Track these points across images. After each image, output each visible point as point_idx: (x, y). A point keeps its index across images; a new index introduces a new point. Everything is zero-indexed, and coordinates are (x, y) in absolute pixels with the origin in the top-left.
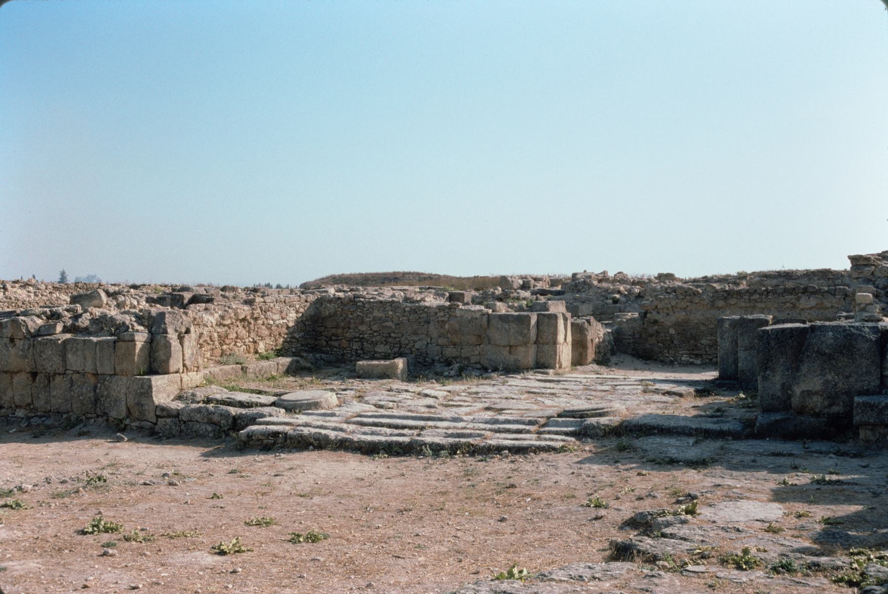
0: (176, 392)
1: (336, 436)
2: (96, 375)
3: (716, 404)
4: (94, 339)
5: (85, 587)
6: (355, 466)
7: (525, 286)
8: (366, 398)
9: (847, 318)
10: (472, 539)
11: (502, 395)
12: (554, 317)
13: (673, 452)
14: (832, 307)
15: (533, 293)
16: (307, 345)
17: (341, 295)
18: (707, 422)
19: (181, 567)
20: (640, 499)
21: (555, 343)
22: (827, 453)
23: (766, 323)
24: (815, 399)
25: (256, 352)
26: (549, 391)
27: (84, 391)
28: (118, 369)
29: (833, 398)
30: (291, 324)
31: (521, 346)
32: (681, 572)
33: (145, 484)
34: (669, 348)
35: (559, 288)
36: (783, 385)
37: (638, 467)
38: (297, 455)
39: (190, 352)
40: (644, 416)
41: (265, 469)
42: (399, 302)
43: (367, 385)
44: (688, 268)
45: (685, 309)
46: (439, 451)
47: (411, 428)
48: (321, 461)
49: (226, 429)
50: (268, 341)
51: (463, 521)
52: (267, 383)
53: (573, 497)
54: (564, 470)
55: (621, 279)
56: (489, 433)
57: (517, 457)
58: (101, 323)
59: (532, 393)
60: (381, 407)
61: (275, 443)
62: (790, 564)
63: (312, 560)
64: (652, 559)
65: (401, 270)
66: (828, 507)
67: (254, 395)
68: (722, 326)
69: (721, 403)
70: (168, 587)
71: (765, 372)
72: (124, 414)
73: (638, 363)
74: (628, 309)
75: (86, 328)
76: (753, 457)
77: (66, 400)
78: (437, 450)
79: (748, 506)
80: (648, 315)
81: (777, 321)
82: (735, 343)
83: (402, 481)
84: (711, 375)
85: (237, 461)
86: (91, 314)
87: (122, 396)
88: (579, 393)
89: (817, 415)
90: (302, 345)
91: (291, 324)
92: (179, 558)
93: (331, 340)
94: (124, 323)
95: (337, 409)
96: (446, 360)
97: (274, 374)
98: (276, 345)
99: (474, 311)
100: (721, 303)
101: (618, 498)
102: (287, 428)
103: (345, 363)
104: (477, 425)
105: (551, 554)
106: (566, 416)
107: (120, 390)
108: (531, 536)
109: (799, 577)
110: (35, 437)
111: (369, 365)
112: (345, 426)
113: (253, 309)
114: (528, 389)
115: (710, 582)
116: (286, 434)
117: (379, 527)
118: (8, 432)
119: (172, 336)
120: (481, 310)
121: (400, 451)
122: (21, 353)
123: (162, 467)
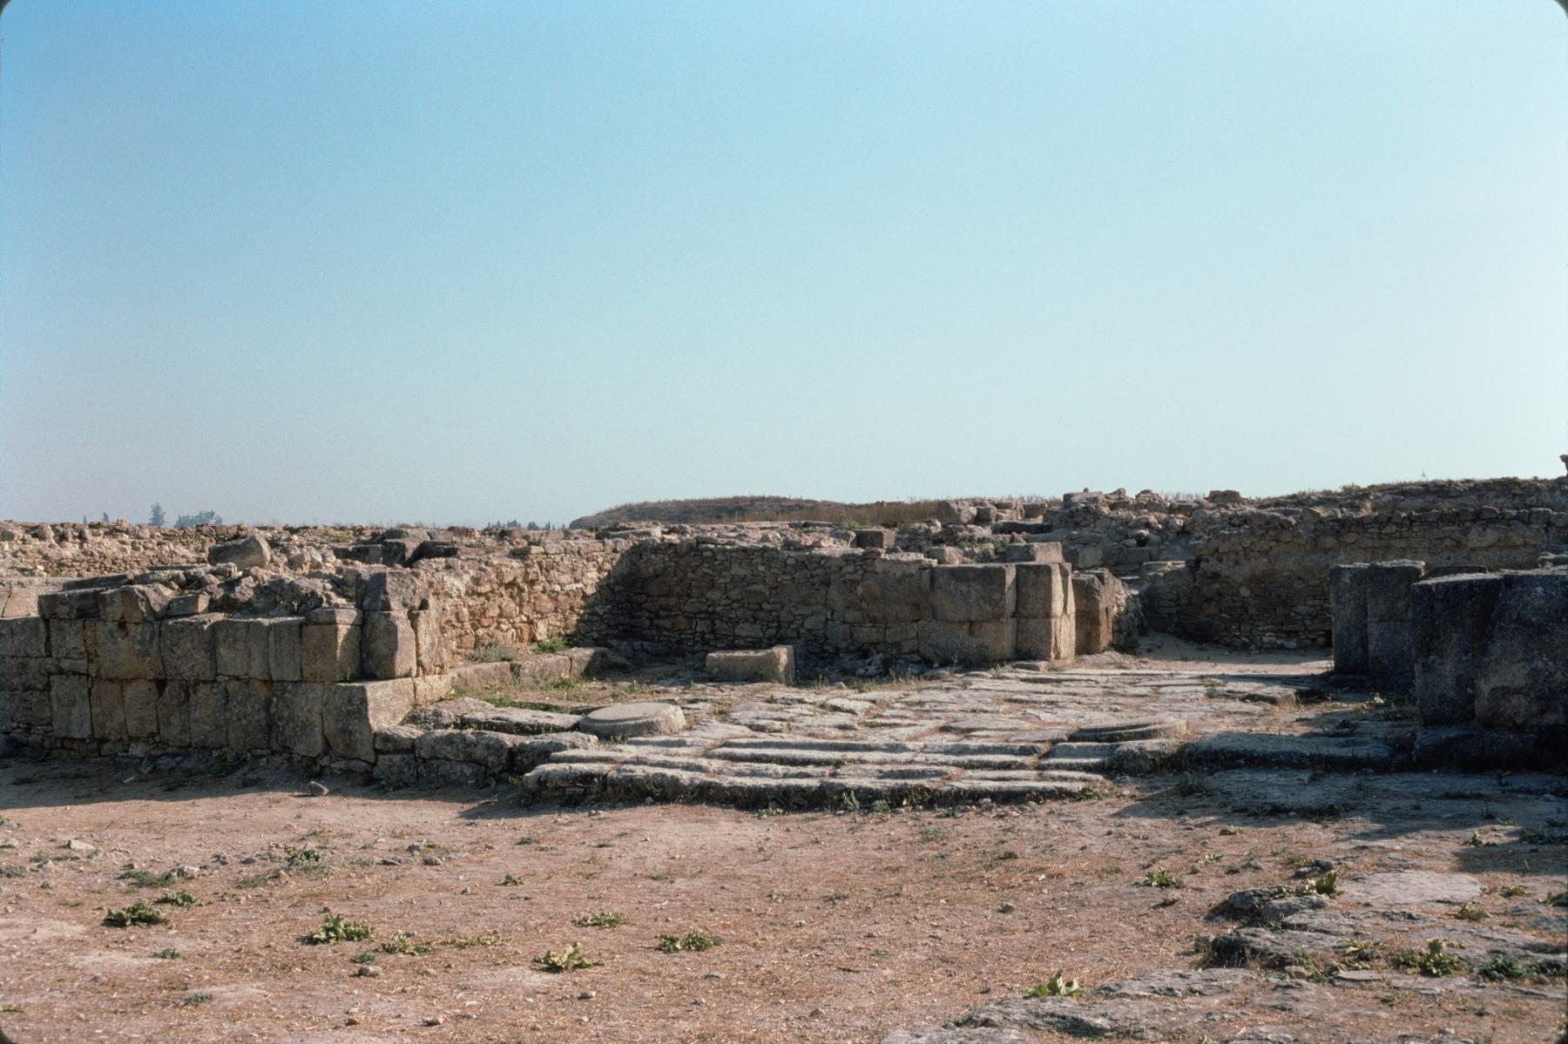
1: (692, 780)
2: (269, 682)
4: (266, 622)
5: (351, 1023)
6: (728, 831)
7: (981, 518)
9: (1556, 562)
11: (965, 706)
12: (1047, 570)
13: (1276, 796)
14: (1525, 545)
16: (617, 626)
17: (674, 538)
19: (494, 991)
20: (1232, 871)
21: (1048, 615)
22: (1539, 793)
23: (1414, 574)
24: (1515, 701)
25: (533, 640)
26: (1044, 698)
28: (306, 673)
29: (1546, 700)
30: (590, 591)
31: (989, 621)
32: (1331, 982)
33: (385, 863)
35: (1039, 520)
36: (1459, 678)
37: (1220, 821)
38: (627, 812)
39: (428, 640)
40: (1220, 736)
42: (774, 549)
43: (730, 693)
44: (1264, 479)
45: (1266, 553)
46: (871, 801)
47: (818, 763)
48: (670, 822)
49: (496, 770)
50: (552, 620)
52: (554, 691)
53: (1118, 871)
55: (1148, 502)
56: (953, 770)
57: (1007, 808)
58: (274, 594)
59: (1016, 701)
60: (761, 729)
61: (585, 794)
62: (1510, 965)
64: (1279, 964)
66: (1555, 878)
67: (540, 713)
69: (1345, 713)
70: (485, 1022)
71: (1426, 657)
73: (1187, 647)
75: (249, 603)
76: (1414, 802)
77: (217, 727)
78: (867, 799)
79: (1420, 882)
80: (1203, 565)
81: (1433, 573)
82: (1363, 609)
84: (1319, 666)
85: (526, 824)
86: (256, 578)
87: (316, 718)
88: (1097, 700)
89: (1520, 729)
90: (609, 627)
91: (590, 591)
92: (486, 977)
93: (658, 616)
94: (313, 593)
95: (686, 734)
96: (859, 649)
97: (565, 676)
98: (566, 628)
99: (907, 563)
100: (1330, 542)
101: (1194, 872)
103: (683, 656)
104: (931, 757)
106: (1084, 739)
107: (312, 708)
108: (1060, 934)
109: (1527, 985)
110: (169, 790)
111: (730, 659)
112: (704, 762)
113: (527, 566)
114: (1008, 695)
115: (1383, 995)
116: (605, 777)
117: (801, 925)
118: (120, 782)
119: (399, 613)
121: (803, 802)
123: (401, 836)
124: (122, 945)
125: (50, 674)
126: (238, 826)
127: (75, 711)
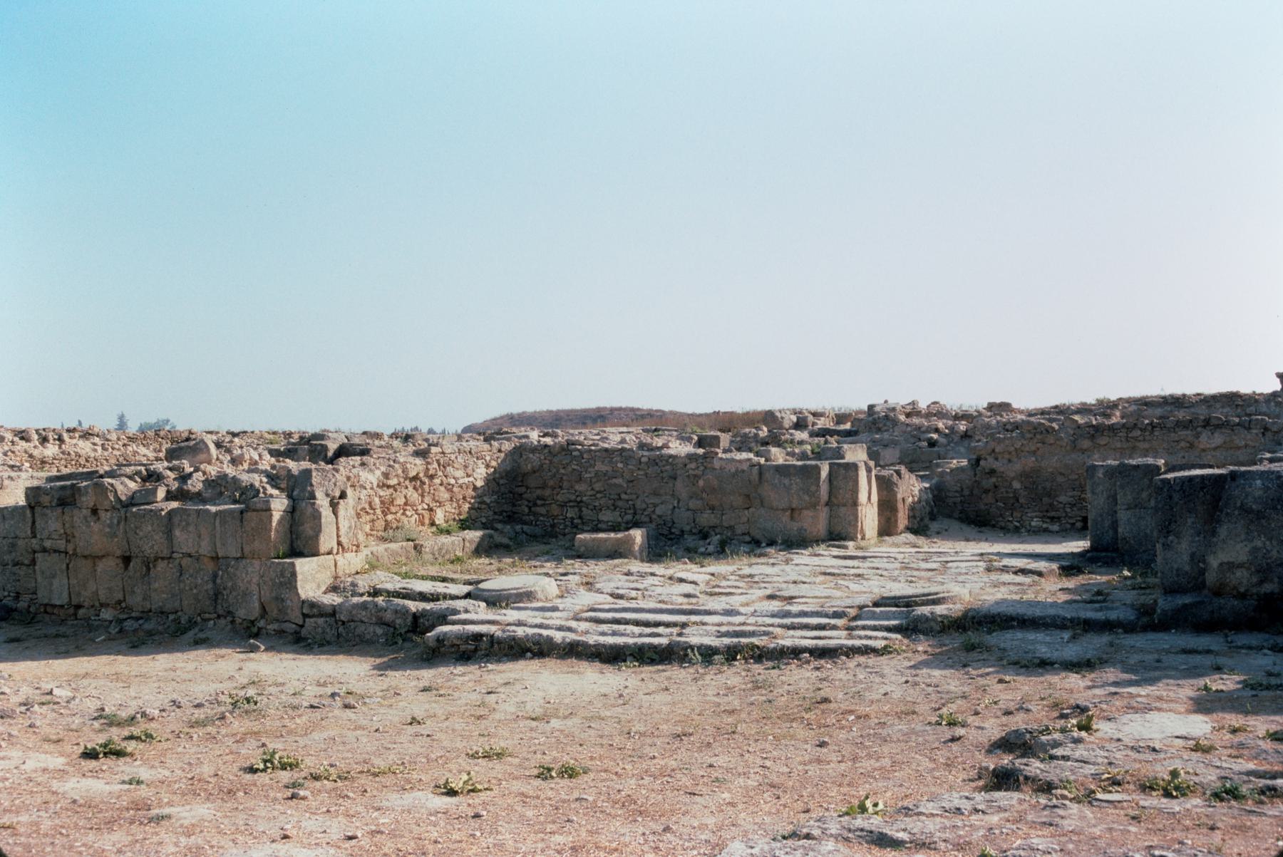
0: (329, 581)
1: (564, 638)
3: (1093, 585)
4: (213, 509)
5: (286, 837)
7: (800, 425)
8: (598, 586)
9: (1271, 461)
10: (786, 770)
13: (1044, 651)
14: (1246, 446)
15: (812, 434)
17: (548, 440)
18: (1086, 610)
20: (1008, 713)
21: (855, 503)
24: (1239, 573)
25: (433, 524)
26: (852, 571)
27: (200, 581)
28: (247, 549)
29: (1264, 572)
30: (480, 484)
31: (807, 508)
32: (1090, 802)
34: (1013, 509)
35: (848, 426)
36: (1193, 555)
37: (997, 672)
40: (997, 603)
41: (470, 684)
42: (631, 450)
43: (595, 568)
44: (1032, 393)
45: (1034, 453)
46: (710, 656)
47: (667, 625)
50: (448, 507)
51: (768, 746)
52: (450, 566)
53: (914, 713)
54: (893, 678)
56: (779, 630)
57: (822, 662)
58: (219, 486)
59: (829, 574)
60: (620, 597)
61: (476, 650)
62: (1236, 789)
63: (577, 800)
64: (1047, 788)
65: (608, 406)
66: (1272, 718)
68: (1093, 476)
69: (1099, 584)
72: (256, 612)
74: (951, 454)
75: (199, 494)
76: (1156, 656)
77: (173, 595)
78: (708, 654)
79: (1162, 721)
80: (982, 463)
81: (1172, 469)
82: (1113, 498)
83: (665, 697)
84: (1078, 546)
85: (427, 675)
86: (204, 473)
87: (254, 588)
88: (896, 573)
89: (1243, 596)
90: (495, 513)
91: (480, 484)
92: (395, 800)
93: (535, 505)
94: (252, 485)
95: (559, 600)
96: (700, 532)
97: (459, 554)
98: (460, 514)
99: (740, 461)
100: (1086, 444)
101: (977, 713)
102: (492, 629)
104: (760, 620)
105: (901, 785)
106: (885, 606)
108: (867, 764)
109: (1250, 805)
110: (134, 647)
111: (594, 540)
112: (573, 624)
113: (428, 463)
114: (823, 569)
115: (1132, 813)
116: (492, 636)
117: (654, 757)
119: (322, 502)
120: (749, 460)
121: (655, 656)
122: (107, 530)
123: (324, 685)
124: (95, 774)
125: (35, 552)
126: (190, 676)
127: (56, 582)
